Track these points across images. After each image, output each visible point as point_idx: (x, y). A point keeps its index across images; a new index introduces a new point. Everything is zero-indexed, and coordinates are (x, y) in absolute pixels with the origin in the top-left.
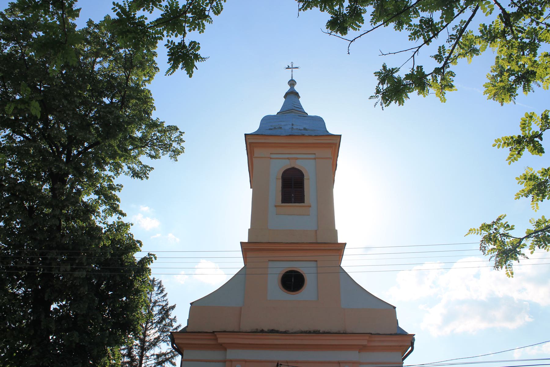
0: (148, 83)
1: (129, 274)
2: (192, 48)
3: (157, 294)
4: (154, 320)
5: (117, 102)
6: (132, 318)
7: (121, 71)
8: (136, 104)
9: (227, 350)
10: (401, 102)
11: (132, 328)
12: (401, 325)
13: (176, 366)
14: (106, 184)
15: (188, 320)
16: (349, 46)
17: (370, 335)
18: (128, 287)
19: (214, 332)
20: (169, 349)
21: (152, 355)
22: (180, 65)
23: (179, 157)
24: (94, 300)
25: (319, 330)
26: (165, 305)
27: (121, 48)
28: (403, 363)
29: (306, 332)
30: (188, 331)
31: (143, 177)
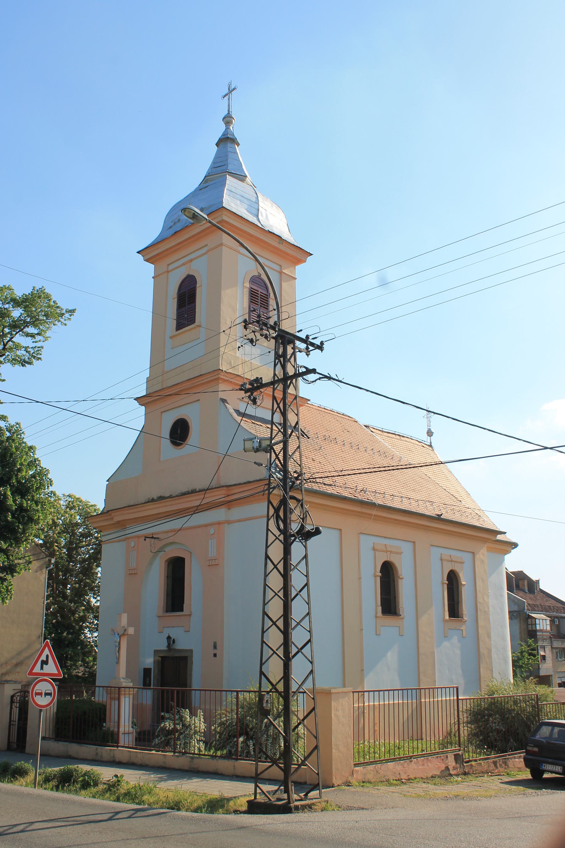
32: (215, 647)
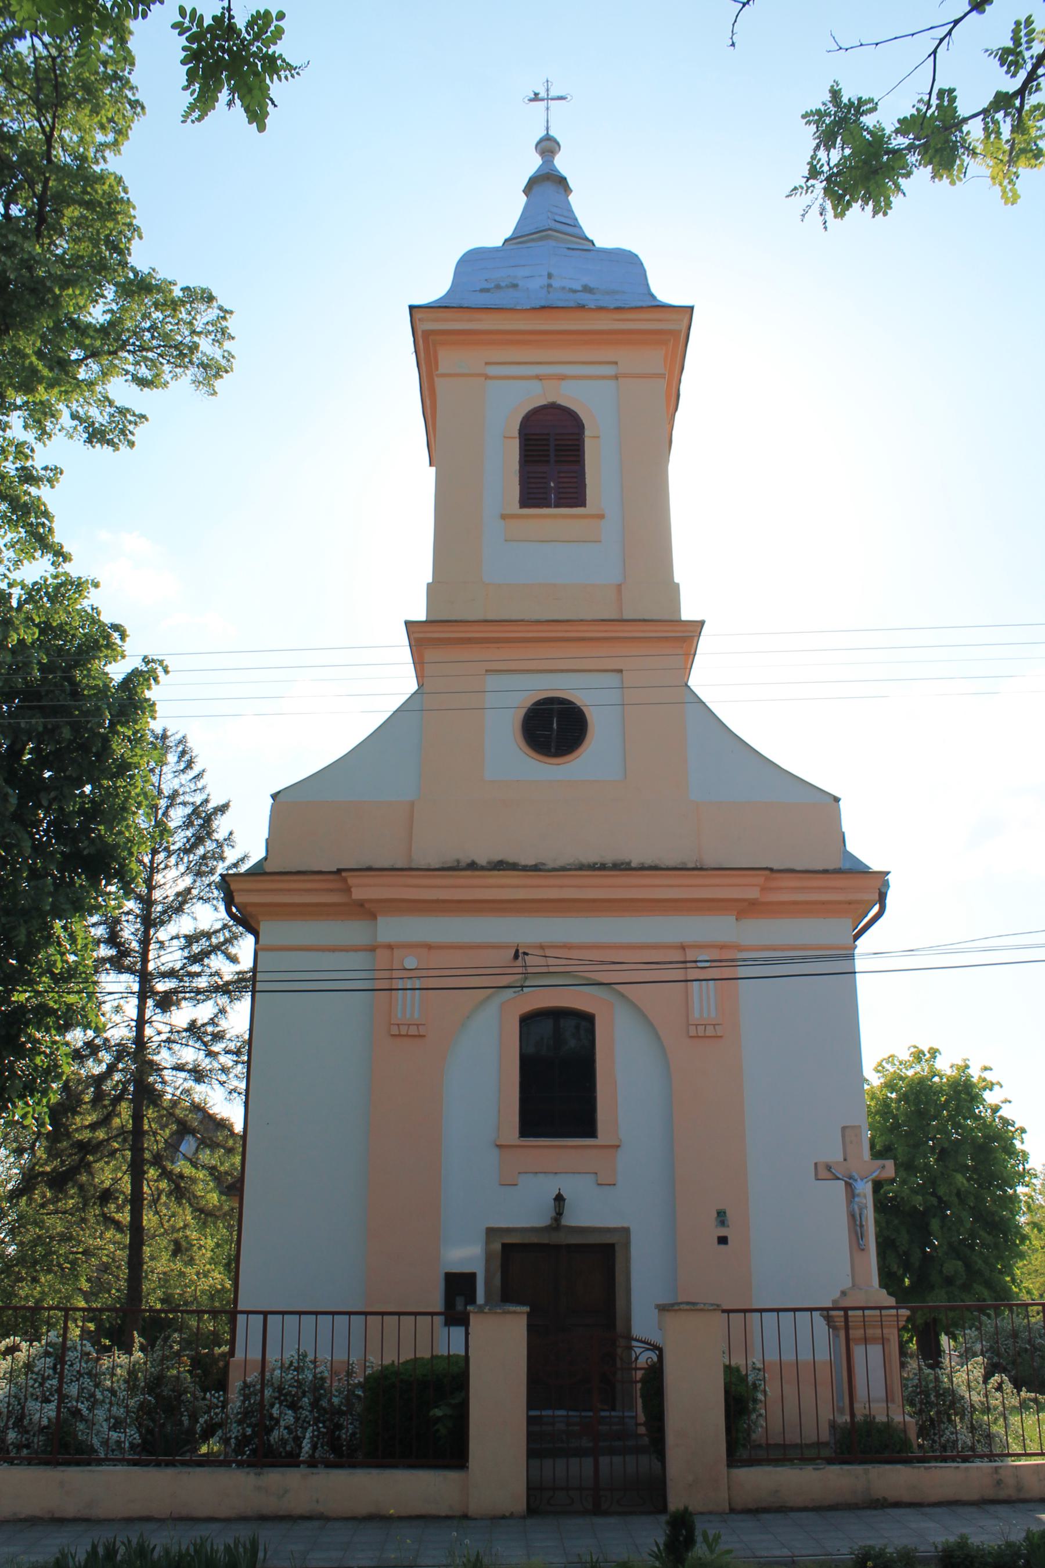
0: (112, 154)
1: (97, 720)
2: (257, 37)
3: (176, 774)
4: (173, 844)
5: (23, 216)
6: (114, 840)
7: (28, 113)
8: (83, 221)
9: (379, 918)
10: (882, 207)
11: (114, 868)
12: (852, 847)
13: (239, 963)
14: (13, 467)
15: (267, 840)
16: (735, 21)
17: (767, 872)
18: (96, 755)
19: (339, 871)
20: (220, 920)
21: (172, 939)
22: (224, 95)
23: (218, 384)
24: (6, 795)
25: (627, 860)
26: (202, 803)
27: (21, 36)
28: (856, 947)
29: (592, 867)
30: (268, 870)
31: (120, 441)
32: (722, 1217)
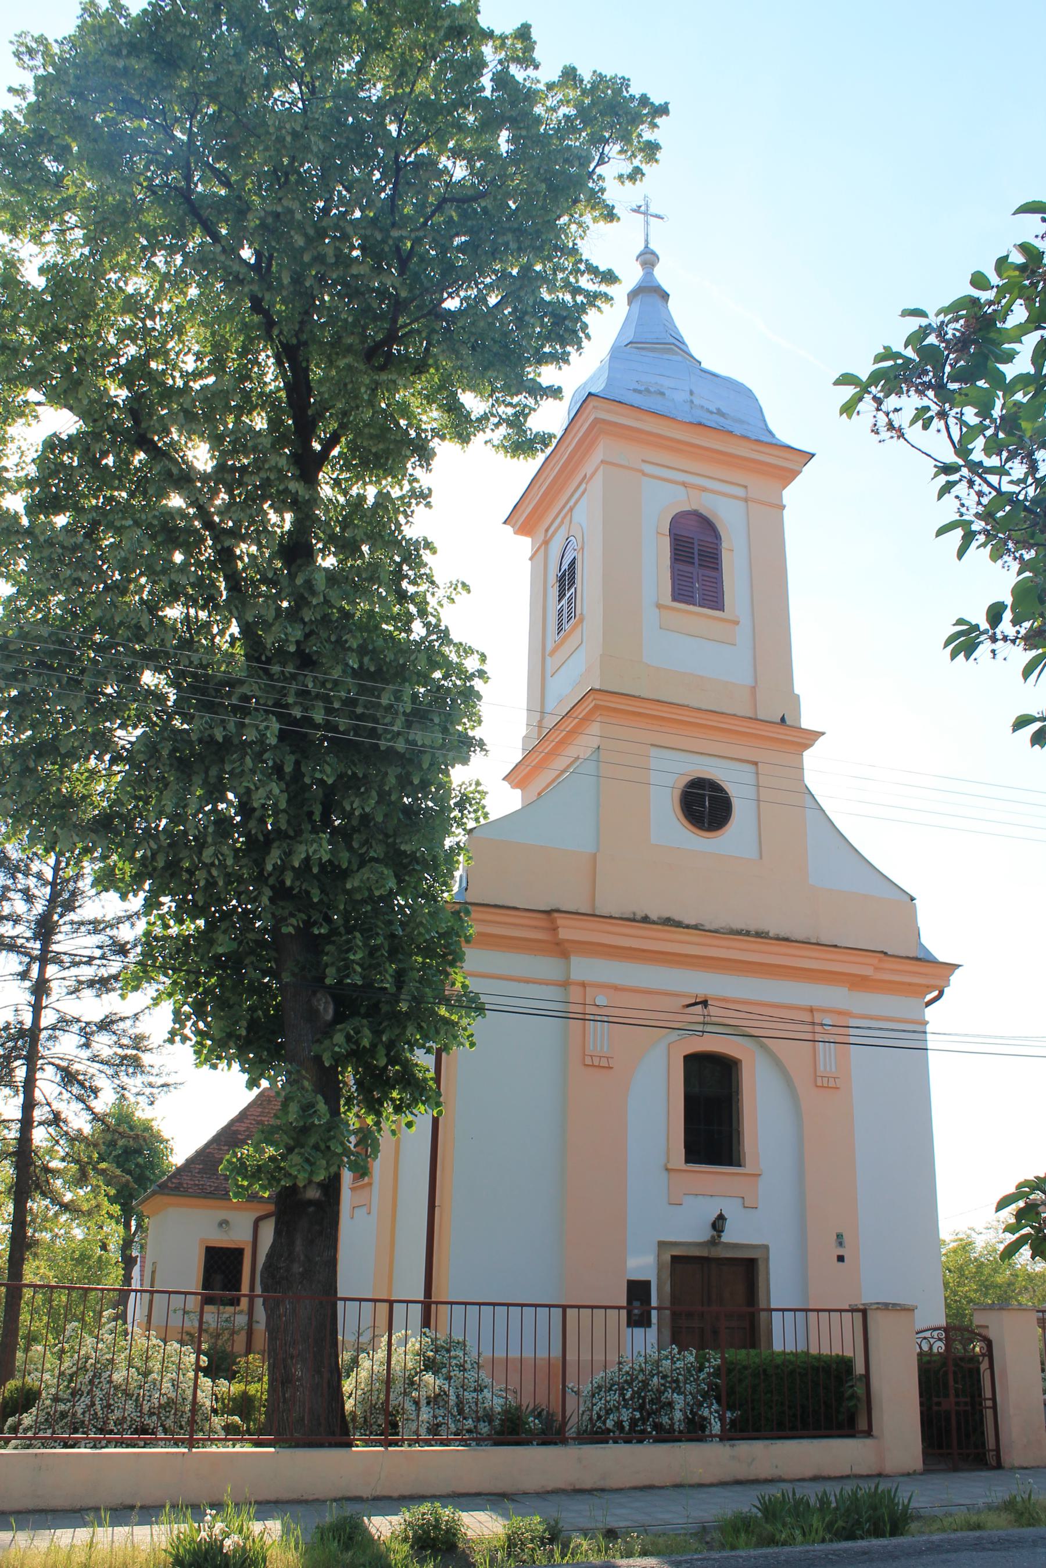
12: (924, 941)
17: (882, 955)
29: (739, 932)
